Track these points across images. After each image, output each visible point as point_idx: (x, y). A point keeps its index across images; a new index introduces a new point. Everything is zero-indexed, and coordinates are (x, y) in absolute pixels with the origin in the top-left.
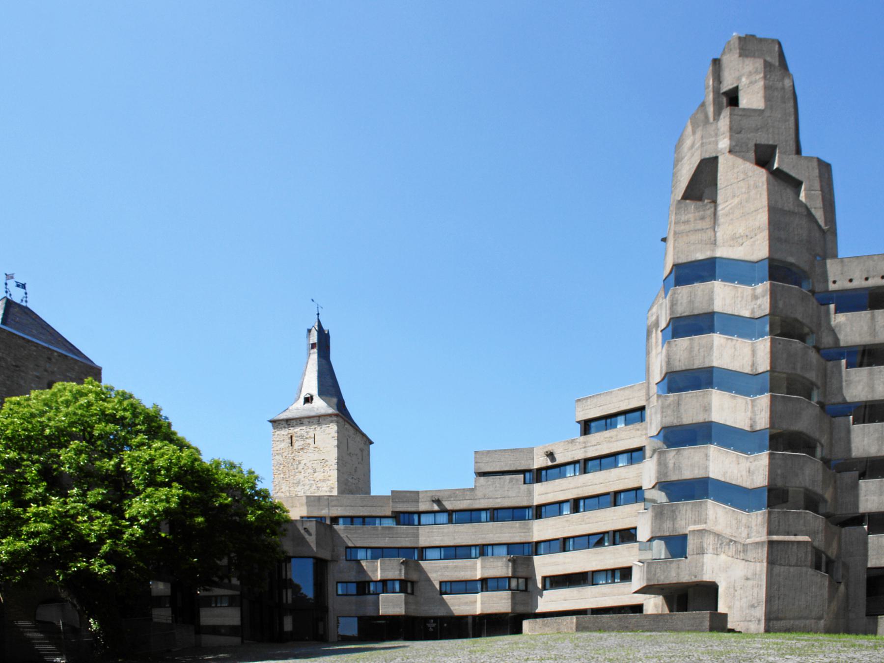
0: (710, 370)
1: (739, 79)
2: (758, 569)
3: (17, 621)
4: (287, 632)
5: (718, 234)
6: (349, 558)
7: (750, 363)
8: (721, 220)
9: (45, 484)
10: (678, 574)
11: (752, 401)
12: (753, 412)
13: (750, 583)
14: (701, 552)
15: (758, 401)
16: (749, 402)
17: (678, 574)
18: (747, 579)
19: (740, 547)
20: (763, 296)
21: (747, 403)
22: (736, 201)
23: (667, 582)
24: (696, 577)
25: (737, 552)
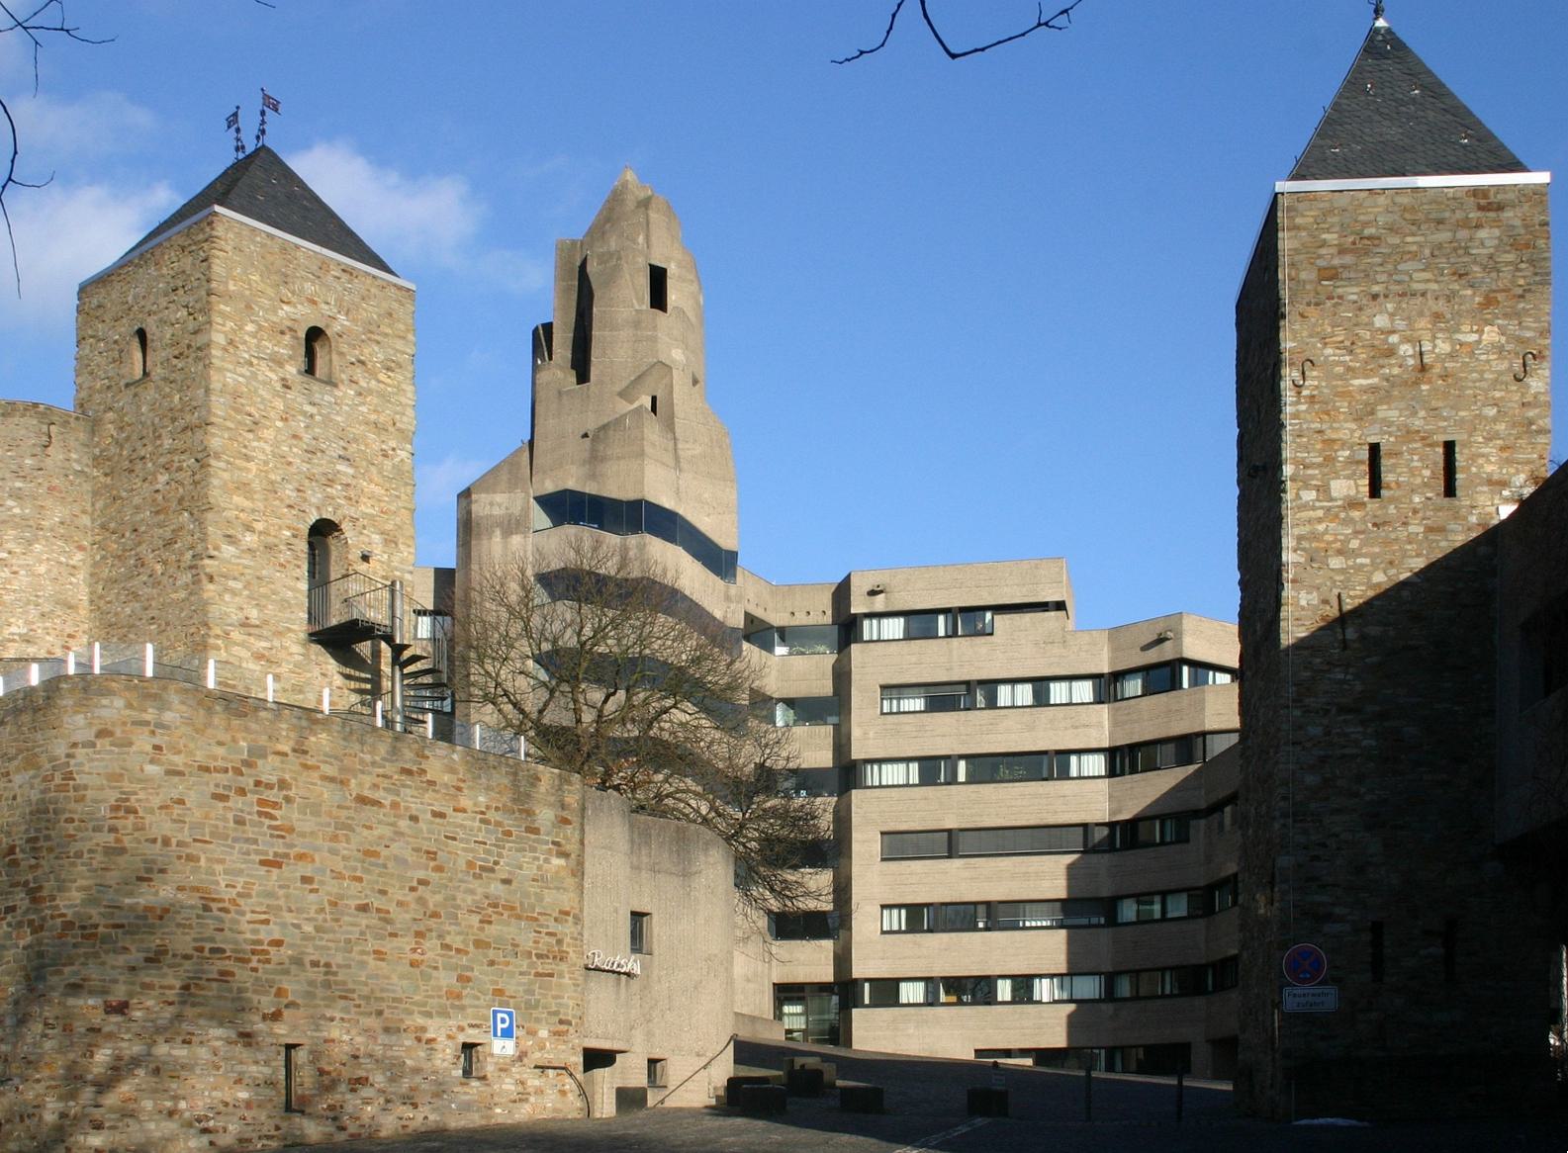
1: (668, 260)
13: (751, 986)
18: (748, 980)
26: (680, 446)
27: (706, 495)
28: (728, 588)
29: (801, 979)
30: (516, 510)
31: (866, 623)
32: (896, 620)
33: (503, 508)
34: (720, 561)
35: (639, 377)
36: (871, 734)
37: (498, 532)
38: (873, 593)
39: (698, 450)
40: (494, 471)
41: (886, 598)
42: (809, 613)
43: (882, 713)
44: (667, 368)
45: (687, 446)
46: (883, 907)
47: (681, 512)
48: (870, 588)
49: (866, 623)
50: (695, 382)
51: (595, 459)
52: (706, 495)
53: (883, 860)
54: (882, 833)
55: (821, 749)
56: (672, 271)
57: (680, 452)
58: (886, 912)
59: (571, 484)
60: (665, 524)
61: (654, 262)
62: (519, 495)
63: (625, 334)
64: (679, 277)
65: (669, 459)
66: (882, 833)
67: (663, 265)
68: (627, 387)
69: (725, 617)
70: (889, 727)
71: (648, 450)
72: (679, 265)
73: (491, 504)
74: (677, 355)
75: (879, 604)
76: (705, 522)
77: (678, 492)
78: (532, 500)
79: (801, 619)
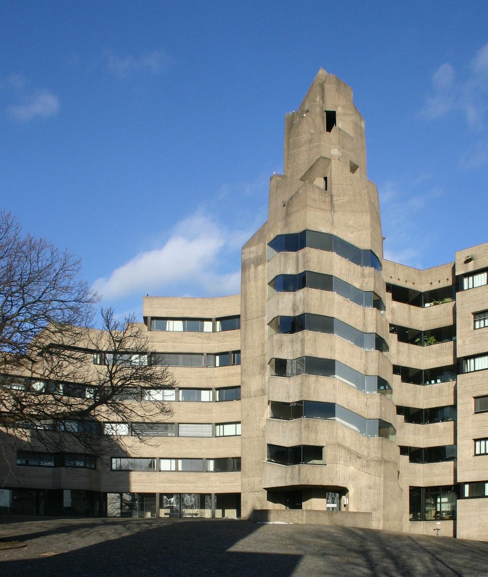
0: (331, 319)
1: (336, 106)
2: (378, 481)
3: (232, 542)
4: (13, 501)
5: (334, 218)
6: (478, 452)
7: (362, 324)
8: (336, 208)
9: (322, 72)
10: (321, 478)
11: (366, 352)
12: (366, 361)
13: (372, 491)
14: (335, 461)
15: (370, 353)
16: (364, 353)
17: (321, 478)
18: (370, 488)
19: (364, 462)
20: (369, 277)
21: (361, 353)
22: (346, 199)
23: (314, 483)
24: (332, 481)
25: (362, 466)
26: (335, 199)
27: (351, 222)
28: (363, 270)
29: (436, 484)
30: (260, 253)
31: (465, 280)
32: (482, 275)
33: (255, 253)
34: (370, 259)
35: (311, 168)
36: (467, 342)
37: (253, 266)
38: (468, 261)
39: (346, 199)
40: (253, 238)
41: (474, 263)
42: (440, 281)
43: (475, 329)
44: (327, 160)
45: (340, 198)
46: (476, 440)
47: (335, 233)
48: (464, 260)
49: (465, 280)
50: (354, 168)
51: (288, 215)
52: (351, 222)
53: (476, 413)
54: (475, 398)
55: (447, 355)
56: (339, 111)
57: (335, 202)
58: (478, 443)
59: (279, 232)
60: (330, 243)
61: (328, 109)
62: (262, 244)
63: (304, 148)
64: (344, 114)
65: (327, 207)
66: (475, 398)
67: (333, 110)
68: (305, 174)
69: (362, 286)
70: (476, 336)
71: (309, 202)
72: (344, 107)
73: (250, 253)
74: (335, 152)
75: (471, 267)
76: (350, 237)
77: (332, 223)
78: (267, 246)
79: (436, 286)
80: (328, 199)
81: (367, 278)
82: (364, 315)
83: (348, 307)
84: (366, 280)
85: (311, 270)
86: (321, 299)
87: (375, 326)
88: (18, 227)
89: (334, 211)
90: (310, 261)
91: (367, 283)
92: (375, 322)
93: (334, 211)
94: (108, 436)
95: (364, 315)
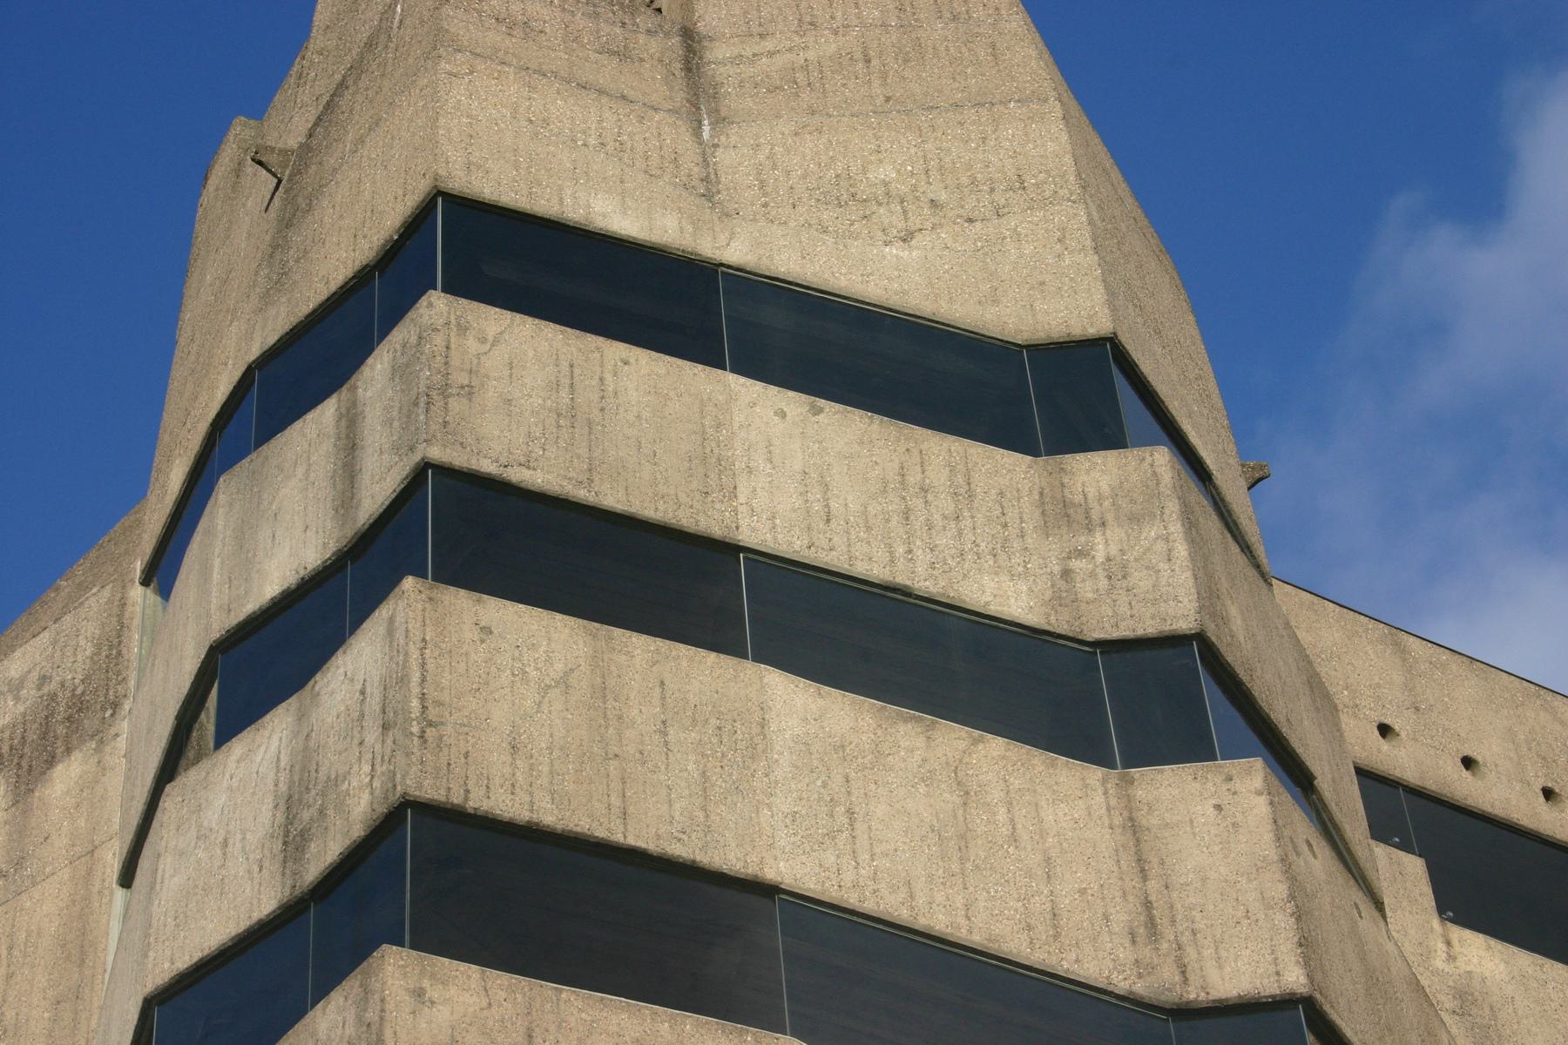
5: (724, 158)
7: (1122, 915)
26: (718, 53)
45: (769, 45)
52: (886, 172)
65: (655, 81)
77: (708, 189)
80: (658, 47)
81: (1116, 533)
82: (1133, 827)
83: (928, 779)
84: (1103, 545)
85: (487, 467)
86: (602, 691)
87: (1284, 921)
88: (590, 424)
89: (720, 121)
90: (469, 392)
91: (1117, 571)
92: (1281, 890)
93: (720, 121)
94: (395, 582)
95: (1133, 827)
